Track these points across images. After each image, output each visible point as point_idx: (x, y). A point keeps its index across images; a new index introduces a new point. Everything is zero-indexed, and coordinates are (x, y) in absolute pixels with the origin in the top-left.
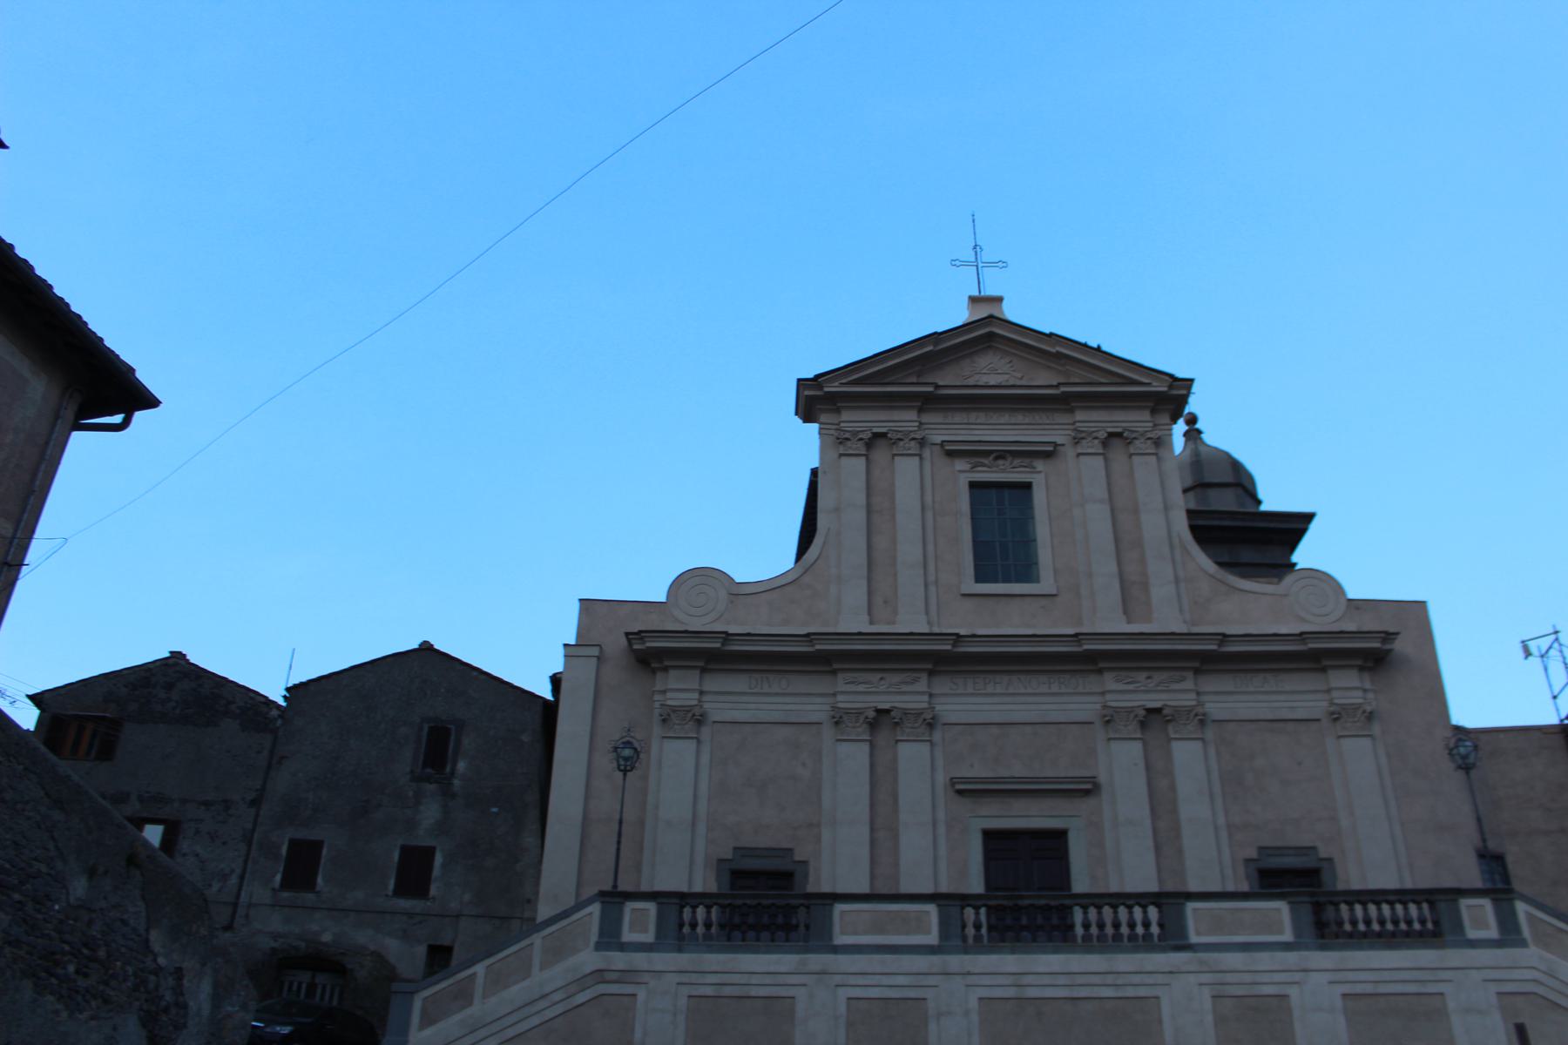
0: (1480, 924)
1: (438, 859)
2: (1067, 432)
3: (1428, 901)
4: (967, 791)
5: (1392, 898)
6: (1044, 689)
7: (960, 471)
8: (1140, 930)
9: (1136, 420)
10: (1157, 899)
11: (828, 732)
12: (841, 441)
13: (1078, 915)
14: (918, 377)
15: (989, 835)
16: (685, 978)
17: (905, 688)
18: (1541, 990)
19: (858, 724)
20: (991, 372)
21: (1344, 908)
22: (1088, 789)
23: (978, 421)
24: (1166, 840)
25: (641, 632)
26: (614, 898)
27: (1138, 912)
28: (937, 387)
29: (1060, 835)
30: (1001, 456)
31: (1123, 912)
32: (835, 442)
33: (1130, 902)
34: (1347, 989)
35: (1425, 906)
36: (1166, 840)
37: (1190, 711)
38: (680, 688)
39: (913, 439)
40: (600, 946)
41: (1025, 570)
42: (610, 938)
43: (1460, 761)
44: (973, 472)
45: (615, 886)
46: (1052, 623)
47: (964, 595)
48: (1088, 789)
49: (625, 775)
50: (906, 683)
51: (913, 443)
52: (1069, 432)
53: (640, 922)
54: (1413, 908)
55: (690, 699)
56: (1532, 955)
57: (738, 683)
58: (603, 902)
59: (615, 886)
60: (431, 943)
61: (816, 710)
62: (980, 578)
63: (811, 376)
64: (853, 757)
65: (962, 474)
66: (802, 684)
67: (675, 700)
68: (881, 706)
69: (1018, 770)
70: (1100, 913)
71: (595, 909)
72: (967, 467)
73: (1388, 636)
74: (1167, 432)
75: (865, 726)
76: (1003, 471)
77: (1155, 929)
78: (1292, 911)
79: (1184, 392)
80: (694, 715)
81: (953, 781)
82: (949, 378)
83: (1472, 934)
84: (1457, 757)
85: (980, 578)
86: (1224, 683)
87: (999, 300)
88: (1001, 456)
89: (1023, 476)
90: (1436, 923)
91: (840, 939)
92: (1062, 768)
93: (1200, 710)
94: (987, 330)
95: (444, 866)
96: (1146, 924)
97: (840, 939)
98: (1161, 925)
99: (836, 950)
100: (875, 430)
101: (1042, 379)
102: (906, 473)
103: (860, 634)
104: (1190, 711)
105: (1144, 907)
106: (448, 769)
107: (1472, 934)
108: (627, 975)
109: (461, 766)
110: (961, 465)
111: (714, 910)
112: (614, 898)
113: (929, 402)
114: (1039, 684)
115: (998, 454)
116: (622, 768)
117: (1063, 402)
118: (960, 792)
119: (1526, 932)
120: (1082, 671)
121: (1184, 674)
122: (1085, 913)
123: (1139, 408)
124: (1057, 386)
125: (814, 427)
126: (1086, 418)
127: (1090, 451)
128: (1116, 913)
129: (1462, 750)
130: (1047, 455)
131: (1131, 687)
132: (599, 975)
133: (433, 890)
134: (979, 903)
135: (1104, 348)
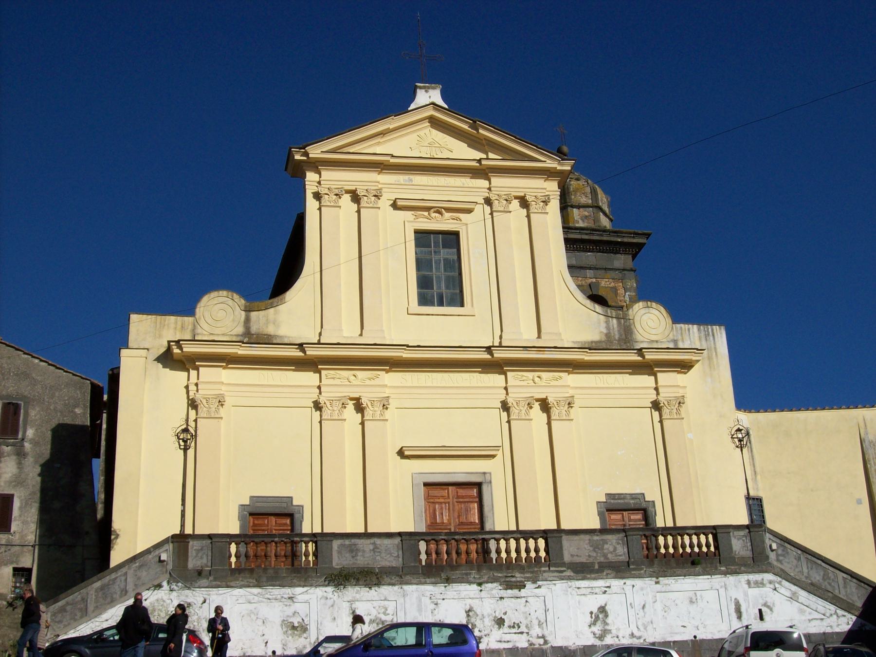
1: (16, 504)
8: (533, 554)
10: (545, 534)
13: (661, 539)
27: (503, 543)
28: (393, 156)
31: (531, 542)
41: (423, 237)
43: (738, 443)
44: (416, 222)
54: (703, 538)
60: (15, 566)
77: (543, 554)
84: (736, 440)
90: (717, 547)
95: (20, 508)
96: (537, 550)
105: (536, 540)
106: (20, 436)
109: (30, 433)
110: (409, 215)
111: (310, 544)
115: (436, 209)
128: (498, 544)
129: (740, 436)
133: (14, 527)
134: (430, 538)
135: (546, 422)
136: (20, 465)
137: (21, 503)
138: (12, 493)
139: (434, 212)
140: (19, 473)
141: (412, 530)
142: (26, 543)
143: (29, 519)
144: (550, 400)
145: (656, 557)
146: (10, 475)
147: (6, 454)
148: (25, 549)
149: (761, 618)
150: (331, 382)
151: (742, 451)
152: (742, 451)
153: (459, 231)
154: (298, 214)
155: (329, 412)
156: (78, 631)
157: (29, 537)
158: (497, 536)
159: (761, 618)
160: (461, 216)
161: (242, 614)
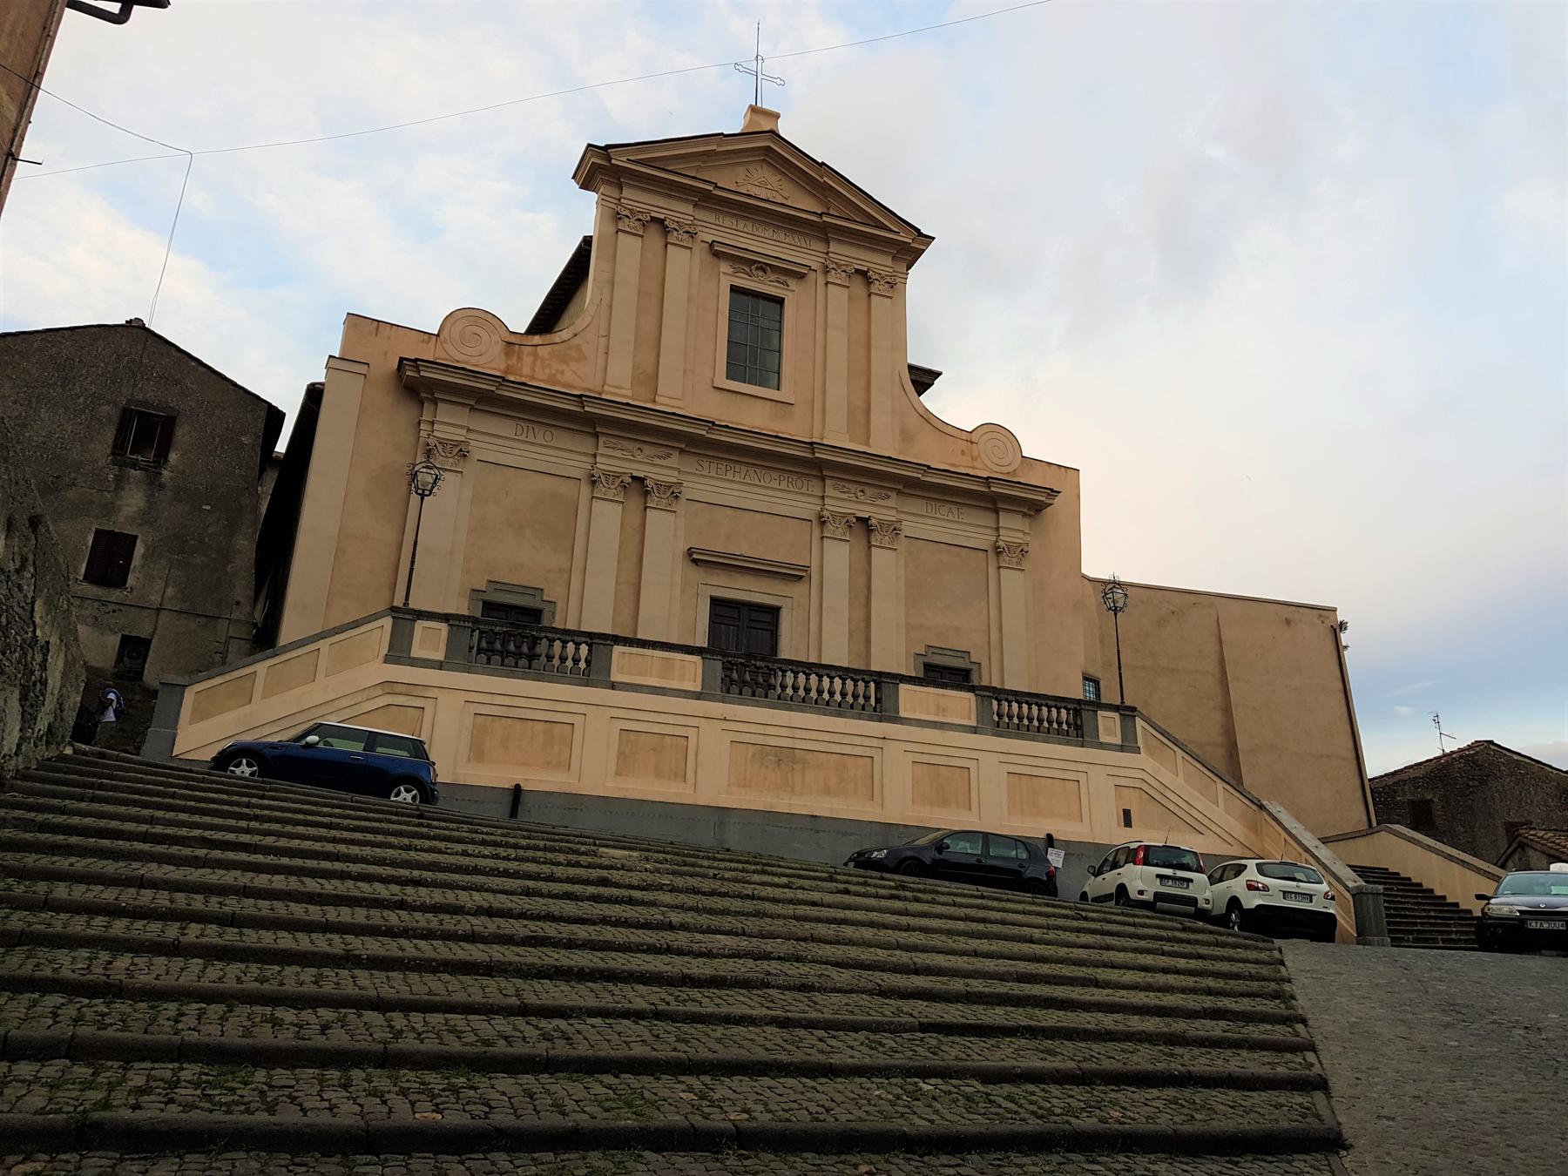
0: (1109, 732)
1: (140, 549)
2: (610, 205)
3: (874, 681)
4: (695, 558)
5: (1050, 703)
6: (775, 484)
7: (724, 273)
9: (878, 262)
11: (585, 490)
12: (617, 217)
14: (697, 172)
15: (715, 602)
16: (1004, 758)
17: (657, 461)
18: (1145, 787)
19: (613, 487)
20: (762, 185)
21: (790, 675)
22: (794, 575)
23: (745, 230)
24: (863, 630)
25: (417, 360)
26: (405, 616)
28: (716, 187)
29: (775, 611)
30: (763, 268)
32: (615, 216)
33: (821, 671)
34: (1013, 769)
35: (872, 685)
36: (863, 630)
37: (670, 487)
38: (450, 422)
39: (639, 220)
40: (388, 659)
42: (398, 653)
45: (1122, 702)
46: (795, 428)
47: (715, 387)
48: (794, 575)
49: (422, 499)
50: (660, 457)
51: (637, 223)
52: (614, 206)
53: (430, 640)
55: (458, 435)
56: (1143, 760)
57: (506, 428)
58: (394, 618)
59: (1122, 702)
61: (805, 506)
62: (731, 375)
63: (602, 144)
64: (837, 558)
65: (728, 276)
66: (565, 440)
67: (442, 432)
68: (636, 474)
69: (745, 549)
70: (807, 679)
71: (387, 622)
72: (730, 270)
73: (1053, 493)
74: (903, 281)
75: (619, 488)
76: (760, 282)
78: (449, 632)
79: (922, 247)
80: (461, 450)
81: (690, 552)
82: (803, 203)
83: (1103, 738)
85: (731, 375)
86: (918, 506)
87: (777, 116)
88: (763, 268)
89: (781, 291)
91: (616, 677)
92: (779, 552)
93: (897, 525)
94: (766, 144)
95: (144, 556)
97: (616, 677)
98: (588, 662)
99: (613, 686)
100: (653, 214)
101: (803, 203)
102: (683, 264)
103: (889, 458)
104: (670, 487)
107: (1103, 738)
108: (410, 688)
110: (725, 267)
112: (405, 616)
113: (706, 199)
114: (772, 480)
116: (420, 491)
117: (822, 232)
118: (695, 561)
119: (1140, 743)
120: (573, 430)
121: (889, 493)
122: (796, 678)
123: (687, 201)
124: (820, 215)
125: (592, 197)
126: (842, 252)
127: (836, 281)
130: (801, 276)
131: (845, 496)
132: (388, 686)
136: (150, 500)
137: (147, 550)
138: (134, 533)
139: (757, 268)
140: (149, 508)
141: (845, 665)
142: (147, 605)
143: (155, 573)
144: (873, 521)
145: (852, 707)
146: (135, 509)
147: (132, 480)
148: (145, 613)
149: (1128, 822)
150: (610, 452)
151: (1116, 614)
152: (1116, 614)
153: (784, 299)
154: (585, 237)
155: (603, 489)
156: (101, 1166)
157: (153, 598)
158: (1050, 703)
159: (1128, 822)
160: (790, 281)
161: (22, 521)
